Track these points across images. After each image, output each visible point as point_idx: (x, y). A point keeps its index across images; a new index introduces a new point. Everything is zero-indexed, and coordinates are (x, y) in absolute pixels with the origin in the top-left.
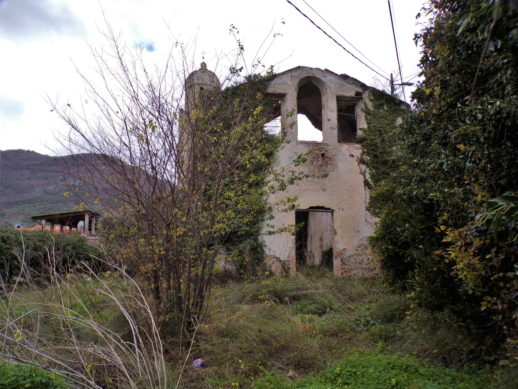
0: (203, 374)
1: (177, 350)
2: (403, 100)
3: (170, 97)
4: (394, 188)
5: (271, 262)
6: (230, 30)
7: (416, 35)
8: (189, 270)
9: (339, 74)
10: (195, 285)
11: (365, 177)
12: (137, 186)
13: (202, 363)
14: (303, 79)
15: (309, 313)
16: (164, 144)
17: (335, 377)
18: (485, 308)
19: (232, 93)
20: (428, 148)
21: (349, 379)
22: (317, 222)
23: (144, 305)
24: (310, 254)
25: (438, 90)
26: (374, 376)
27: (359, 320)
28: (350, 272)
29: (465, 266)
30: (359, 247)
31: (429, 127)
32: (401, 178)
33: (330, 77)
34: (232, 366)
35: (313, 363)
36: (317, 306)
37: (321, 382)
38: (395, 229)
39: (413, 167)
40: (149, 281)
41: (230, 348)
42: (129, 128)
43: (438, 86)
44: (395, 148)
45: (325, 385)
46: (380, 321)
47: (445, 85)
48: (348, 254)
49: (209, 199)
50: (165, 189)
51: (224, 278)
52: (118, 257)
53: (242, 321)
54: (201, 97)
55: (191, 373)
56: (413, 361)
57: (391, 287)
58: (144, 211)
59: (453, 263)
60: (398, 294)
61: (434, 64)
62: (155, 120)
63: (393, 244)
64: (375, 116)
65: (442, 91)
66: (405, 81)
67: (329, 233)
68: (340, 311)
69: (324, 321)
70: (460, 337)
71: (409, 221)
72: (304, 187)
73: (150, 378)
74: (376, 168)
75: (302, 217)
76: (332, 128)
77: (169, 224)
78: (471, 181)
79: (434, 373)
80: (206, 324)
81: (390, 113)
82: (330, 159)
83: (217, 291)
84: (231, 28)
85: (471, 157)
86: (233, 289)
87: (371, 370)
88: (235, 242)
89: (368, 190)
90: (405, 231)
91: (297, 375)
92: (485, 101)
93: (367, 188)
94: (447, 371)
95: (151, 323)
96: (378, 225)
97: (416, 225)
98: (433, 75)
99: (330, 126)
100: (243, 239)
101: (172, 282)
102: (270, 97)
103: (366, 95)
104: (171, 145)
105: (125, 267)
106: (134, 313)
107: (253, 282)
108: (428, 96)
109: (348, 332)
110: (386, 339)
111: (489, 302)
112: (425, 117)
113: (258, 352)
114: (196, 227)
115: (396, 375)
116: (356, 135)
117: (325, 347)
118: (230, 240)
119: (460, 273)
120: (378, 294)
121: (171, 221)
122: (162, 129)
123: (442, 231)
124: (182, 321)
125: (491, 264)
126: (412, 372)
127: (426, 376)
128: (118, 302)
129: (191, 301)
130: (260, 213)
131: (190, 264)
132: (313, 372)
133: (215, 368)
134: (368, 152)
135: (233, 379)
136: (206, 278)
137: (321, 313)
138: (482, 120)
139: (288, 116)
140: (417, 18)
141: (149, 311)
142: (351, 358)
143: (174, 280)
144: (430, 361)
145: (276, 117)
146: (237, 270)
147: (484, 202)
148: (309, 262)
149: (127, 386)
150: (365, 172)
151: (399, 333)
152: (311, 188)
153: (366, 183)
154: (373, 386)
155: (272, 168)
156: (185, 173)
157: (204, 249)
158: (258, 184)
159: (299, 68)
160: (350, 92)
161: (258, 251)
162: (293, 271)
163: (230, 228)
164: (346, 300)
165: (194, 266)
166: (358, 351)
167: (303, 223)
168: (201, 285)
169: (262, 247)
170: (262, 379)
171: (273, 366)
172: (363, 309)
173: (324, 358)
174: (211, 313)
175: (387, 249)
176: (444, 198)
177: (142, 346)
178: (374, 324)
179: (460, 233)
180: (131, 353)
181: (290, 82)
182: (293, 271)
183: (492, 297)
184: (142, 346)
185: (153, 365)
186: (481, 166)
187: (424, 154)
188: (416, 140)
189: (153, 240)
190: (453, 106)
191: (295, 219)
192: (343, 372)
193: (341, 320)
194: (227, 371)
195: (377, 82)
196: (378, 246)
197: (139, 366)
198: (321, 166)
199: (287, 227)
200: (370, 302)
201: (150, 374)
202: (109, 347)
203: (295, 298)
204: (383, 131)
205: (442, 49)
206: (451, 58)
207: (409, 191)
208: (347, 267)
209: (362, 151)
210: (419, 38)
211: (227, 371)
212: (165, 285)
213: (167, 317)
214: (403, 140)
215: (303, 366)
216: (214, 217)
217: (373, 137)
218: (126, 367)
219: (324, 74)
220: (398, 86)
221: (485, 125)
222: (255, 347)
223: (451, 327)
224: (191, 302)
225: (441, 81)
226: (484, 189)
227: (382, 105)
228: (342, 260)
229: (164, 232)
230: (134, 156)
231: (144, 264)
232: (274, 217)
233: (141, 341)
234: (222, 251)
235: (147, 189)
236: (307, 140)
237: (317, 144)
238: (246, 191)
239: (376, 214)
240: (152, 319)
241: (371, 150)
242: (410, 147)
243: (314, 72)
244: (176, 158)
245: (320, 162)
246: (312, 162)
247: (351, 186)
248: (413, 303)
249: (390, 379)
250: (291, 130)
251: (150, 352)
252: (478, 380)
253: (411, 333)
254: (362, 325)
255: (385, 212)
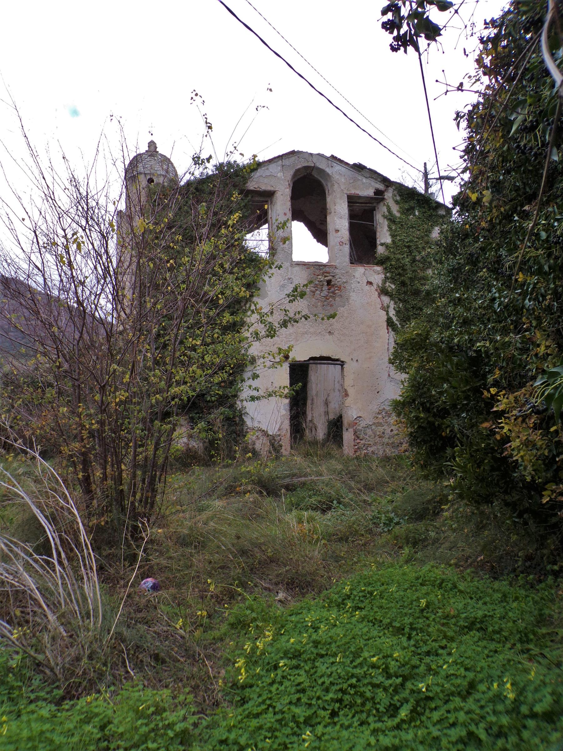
0: (155, 600)
2: (442, 202)
4: (428, 331)
6: (192, 98)
7: (458, 114)
8: (135, 451)
9: (351, 163)
10: (144, 473)
11: (387, 314)
12: (55, 329)
13: (154, 584)
16: (95, 268)
17: (343, 600)
18: (548, 499)
20: (475, 275)
21: (362, 601)
22: (320, 379)
23: (68, 503)
25: (487, 193)
27: (378, 518)
29: (522, 443)
30: (379, 413)
31: (476, 245)
33: (338, 167)
34: (198, 587)
35: (313, 580)
36: (319, 498)
37: (324, 607)
38: (429, 389)
39: (455, 304)
42: (41, 243)
43: (487, 189)
44: (430, 272)
45: (328, 610)
46: (407, 518)
47: (497, 187)
48: (363, 424)
49: (165, 346)
50: (97, 334)
51: (188, 460)
52: (27, 434)
54: (150, 193)
56: (451, 574)
57: (423, 471)
58: (66, 366)
59: (506, 439)
61: (483, 154)
62: (81, 232)
63: (427, 410)
64: (402, 225)
65: (493, 197)
67: (337, 393)
70: (514, 538)
71: (448, 380)
73: (77, 608)
74: (404, 301)
75: (299, 372)
77: (104, 386)
78: (531, 326)
79: (478, 588)
81: (423, 221)
85: (531, 294)
86: (199, 476)
87: (393, 589)
90: (442, 394)
91: (289, 598)
92: (551, 212)
93: (390, 330)
94: (496, 585)
95: (78, 528)
96: (406, 384)
98: (481, 173)
99: (339, 240)
101: (109, 470)
102: (252, 197)
103: (389, 195)
105: (39, 447)
106: (52, 514)
107: (228, 466)
108: (475, 203)
111: (553, 491)
112: (471, 231)
113: (235, 567)
115: (427, 594)
116: (375, 253)
117: (330, 557)
118: (195, 407)
119: (515, 453)
121: (108, 381)
123: (492, 395)
124: (124, 525)
125: (556, 439)
126: (448, 589)
127: (467, 593)
128: (27, 499)
130: (238, 368)
132: (313, 593)
133: (172, 590)
134: (392, 278)
135: (199, 606)
137: (325, 508)
138: (547, 240)
141: (76, 512)
143: (113, 466)
144: (473, 572)
145: (261, 225)
146: (206, 448)
147: (548, 355)
149: (42, 619)
150: (388, 307)
151: (432, 534)
152: (312, 330)
153: (390, 323)
154: (395, 610)
155: (255, 306)
156: (128, 311)
157: (157, 423)
158: (235, 327)
159: (293, 153)
160: (367, 190)
161: (235, 424)
162: (286, 449)
163: (194, 391)
165: (140, 446)
166: (376, 562)
167: (300, 384)
168: (153, 473)
170: (241, 605)
171: (256, 586)
172: (384, 502)
174: (168, 512)
175: (417, 418)
176: (496, 349)
177: (66, 562)
178: (398, 523)
179: (516, 397)
180: (48, 572)
181: (280, 175)
182: (286, 449)
183: (557, 484)
184: (66, 562)
185: (81, 588)
186: (545, 305)
187: (469, 284)
189: (81, 410)
190: (508, 217)
192: (355, 593)
193: (354, 518)
194: (190, 594)
196: (405, 414)
197: (61, 590)
198: (326, 298)
200: (394, 492)
202: (14, 564)
204: (413, 247)
205: (493, 136)
206: (505, 148)
207: (449, 337)
208: (362, 442)
209: (383, 276)
210: (462, 117)
211: (190, 594)
212: (98, 474)
213: (102, 519)
214: (441, 263)
216: (170, 376)
218: (41, 594)
219: (330, 162)
220: (434, 181)
221: (550, 248)
222: (231, 561)
223: (503, 523)
225: (492, 182)
226: (548, 336)
227: (412, 209)
229: (98, 397)
230: (49, 284)
231: (67, 444)
232: (258, 376)
233: (63, 555)
235: (71, 333)
236: (307, 260)
237: (321, 265)
238: (218, 337)
239: (402, 369)
240: (80, 524)
241: (396, 275)
242: (450, 273)
243: (315, 160)
244: (113, 288)
245: (325, 293)
246: (314, 292)
249: (418, 599)
250: (282, 246)
251: (76, 570)
252: (537, 598)
253: (449, 533)
254: (382, 525)
255: (416, 365)
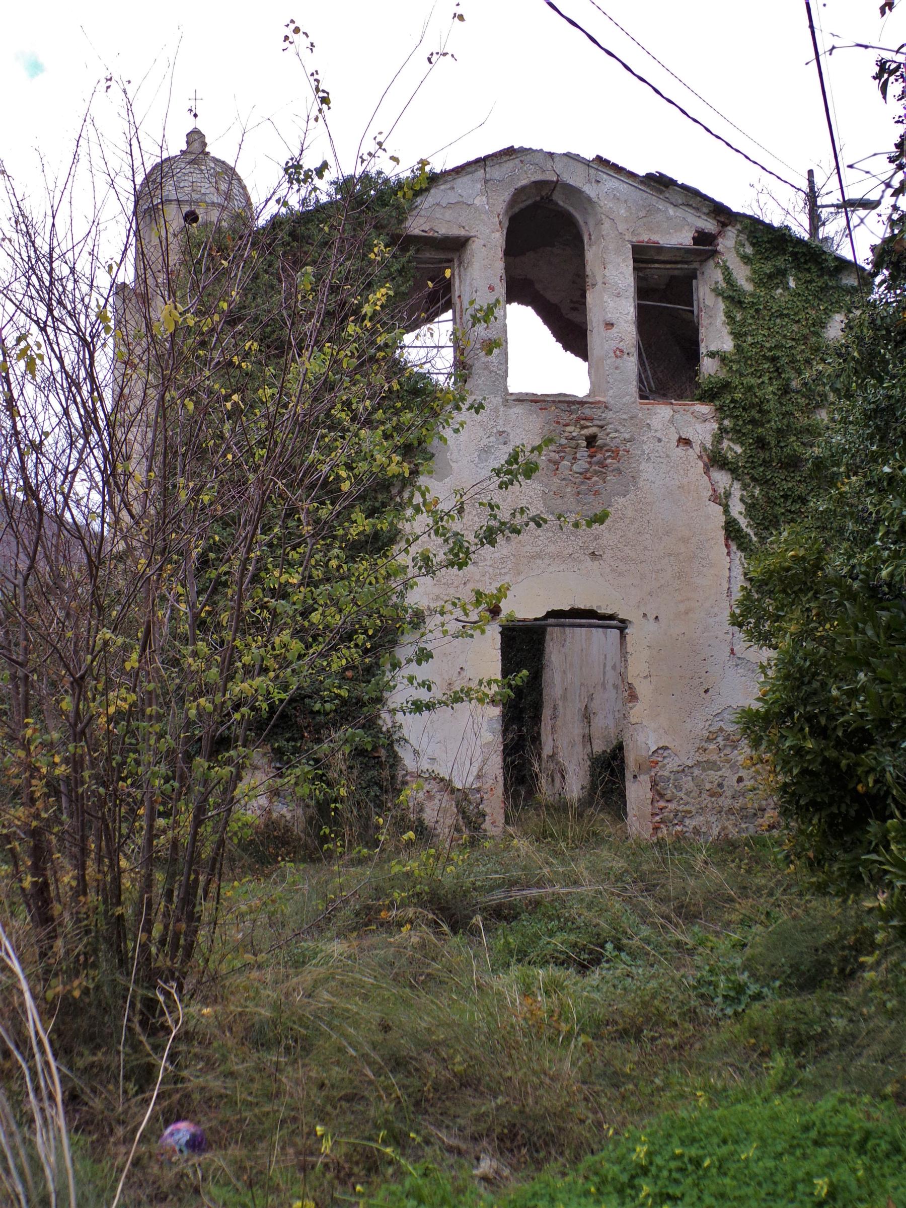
0: (195, 1172)
1: (109, 1091)
2: (850, 257)
3: (85, 254)
5: (421, 795)
6: (286, 38)
8: (151, 827)
9: (642, 172)
10: (171, 877)
11: (726, 511)
14: (523, 189)
15: (547, 962)
16: (66, 412)
17: (633, 1177)
19: (292, 234)
21: (677, 1182)
22: (570, 660)
24: (552, 766)
26: (756, 1170)
27: (710, 983)
28: (681, 822)
30: (709, 740)
32: (844, 516)
33: (611, 183)
34: (294, 1145)
35: (560, 1129)
37: (587, 1193)
40: (16, 865)
41: (288, 1085)
48: (672, 764)
50: (67, 560)
51: (269, 848)
53: (326, 996)
54: (190, 245)
55: (155, 1169)
60: (837, 895)
63: (820, 732)
64: (757, 311)
66: (853, 194)
67: (611, 694)
68: (647, 954)
69: (598, 988)
71: (868, 664)
72: (528, 548)
73: (20, 1189)
75: (524, 645)
76: (619, 353)
77: (82, 677)
80: (205, 1002)
82: (615, 454)
83: (242, 894)
84: (289, 32)
86: (295, 886)
88: (300, 729)
89: (739, 554)
91: (506, 1172)
93: (734, 548)
95: (23, 1004)
96: (771, 673)
97: (890, 677)
99: (614, 345)
100: (330, 723)
102: (417, 251)
103: (729, 243)
104: (90, 417)
107: (361, 861)
109: (675, 1024)
110: (798, 1046)
114: (172, 687)
115: (831, 1165)
116: (697, 373)
117: (598, 1076)
118: (286, 726)
120: (771, 894)
122: (60, 360)
126: (880, 1155)
129: (157, 930)
130: (383, 636)
131: (152, 809)
132: (561, 1160)
133: (236, 1151)
135: (297, 1189)
136: (207, 852)
137: (586, 960)
139: (476, 320)
140: (883, 13)
141: (16, 967)
142: (683, 1114)
143: (100, 861)
148: (546, 790)
150: (728, 495)
151: (839, 1023)
152: (551, 549)
153: (732, 531)
157: (200, 762)
158: (378, 544)
159: (510, 152)
160: (677, 232)
161: (378, 763)
164: (667, 918)
168: (192, 875)
169: (391, 745)
171: (427, 1142)
172: (723, 945)
173: (595, 1112)
174: (224, 968)
175: (799, 751)
178: (758, 997)
181: (480, 201)
185: (30, 1143)
188: (890, 397)
189: (29, 732)
191: (499, 653)
192: (659, 1160)
193: (653, 984)
194: (277, 1162)
195: (763, 198)
196: (771, 743)
198: (585, 475)
199: (474, 685)
200: (746, 922)
201: (21, 1173)
203: (501, 914)
207: (868, 565)
209: (716, 426)
211: (277, 1162)
212: (68, 879)
213: (76, 983)
214: (849, 396)
215: (527, 1140)
216: (232, 655)
217: (753, 381)
219: (592, 171)
222: (370, 1082)
224: (156, 933)
227: (781, 273)
228: (654, 784)
232: (430, 656)
234: (258, 755)
236: (540, 391)
237: (570, 403)
239: (763, 638)
241: (745, 424)
242: (870, 418)
243: (559, 167)
244: (106, 457)
246: (556, 463)
247: (685, 540)
248: (883, 928)
249: (809, 1178)
253: (879, 1021)
254: (719, 1000)
255: (793, 629)
